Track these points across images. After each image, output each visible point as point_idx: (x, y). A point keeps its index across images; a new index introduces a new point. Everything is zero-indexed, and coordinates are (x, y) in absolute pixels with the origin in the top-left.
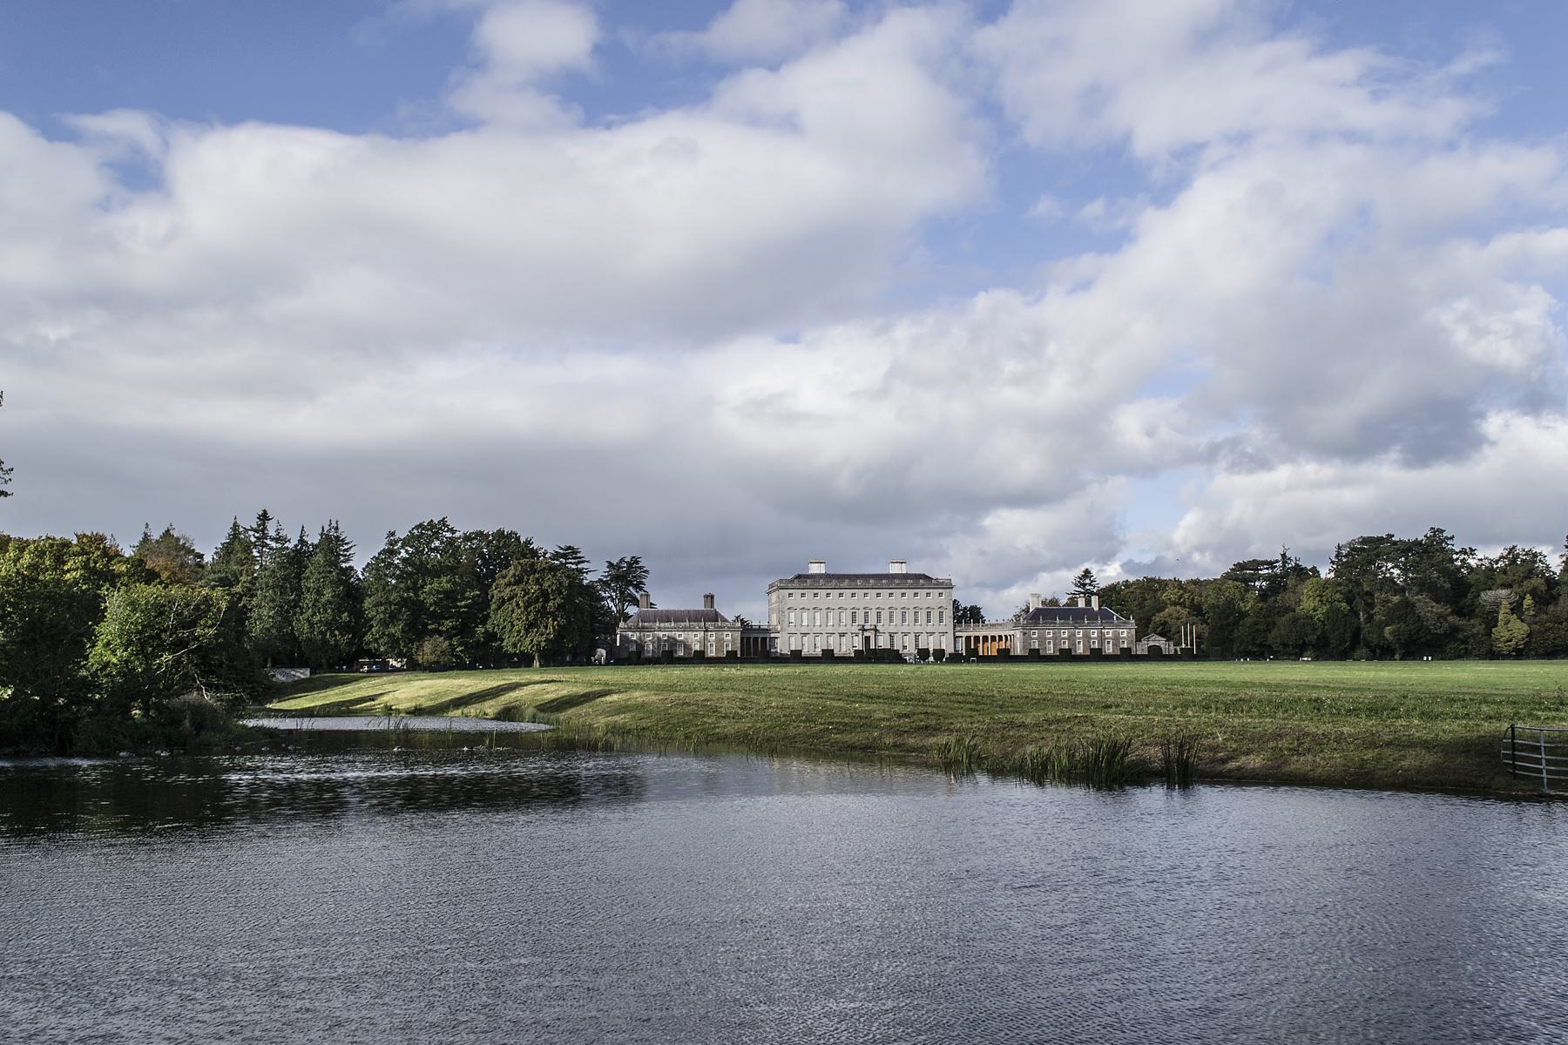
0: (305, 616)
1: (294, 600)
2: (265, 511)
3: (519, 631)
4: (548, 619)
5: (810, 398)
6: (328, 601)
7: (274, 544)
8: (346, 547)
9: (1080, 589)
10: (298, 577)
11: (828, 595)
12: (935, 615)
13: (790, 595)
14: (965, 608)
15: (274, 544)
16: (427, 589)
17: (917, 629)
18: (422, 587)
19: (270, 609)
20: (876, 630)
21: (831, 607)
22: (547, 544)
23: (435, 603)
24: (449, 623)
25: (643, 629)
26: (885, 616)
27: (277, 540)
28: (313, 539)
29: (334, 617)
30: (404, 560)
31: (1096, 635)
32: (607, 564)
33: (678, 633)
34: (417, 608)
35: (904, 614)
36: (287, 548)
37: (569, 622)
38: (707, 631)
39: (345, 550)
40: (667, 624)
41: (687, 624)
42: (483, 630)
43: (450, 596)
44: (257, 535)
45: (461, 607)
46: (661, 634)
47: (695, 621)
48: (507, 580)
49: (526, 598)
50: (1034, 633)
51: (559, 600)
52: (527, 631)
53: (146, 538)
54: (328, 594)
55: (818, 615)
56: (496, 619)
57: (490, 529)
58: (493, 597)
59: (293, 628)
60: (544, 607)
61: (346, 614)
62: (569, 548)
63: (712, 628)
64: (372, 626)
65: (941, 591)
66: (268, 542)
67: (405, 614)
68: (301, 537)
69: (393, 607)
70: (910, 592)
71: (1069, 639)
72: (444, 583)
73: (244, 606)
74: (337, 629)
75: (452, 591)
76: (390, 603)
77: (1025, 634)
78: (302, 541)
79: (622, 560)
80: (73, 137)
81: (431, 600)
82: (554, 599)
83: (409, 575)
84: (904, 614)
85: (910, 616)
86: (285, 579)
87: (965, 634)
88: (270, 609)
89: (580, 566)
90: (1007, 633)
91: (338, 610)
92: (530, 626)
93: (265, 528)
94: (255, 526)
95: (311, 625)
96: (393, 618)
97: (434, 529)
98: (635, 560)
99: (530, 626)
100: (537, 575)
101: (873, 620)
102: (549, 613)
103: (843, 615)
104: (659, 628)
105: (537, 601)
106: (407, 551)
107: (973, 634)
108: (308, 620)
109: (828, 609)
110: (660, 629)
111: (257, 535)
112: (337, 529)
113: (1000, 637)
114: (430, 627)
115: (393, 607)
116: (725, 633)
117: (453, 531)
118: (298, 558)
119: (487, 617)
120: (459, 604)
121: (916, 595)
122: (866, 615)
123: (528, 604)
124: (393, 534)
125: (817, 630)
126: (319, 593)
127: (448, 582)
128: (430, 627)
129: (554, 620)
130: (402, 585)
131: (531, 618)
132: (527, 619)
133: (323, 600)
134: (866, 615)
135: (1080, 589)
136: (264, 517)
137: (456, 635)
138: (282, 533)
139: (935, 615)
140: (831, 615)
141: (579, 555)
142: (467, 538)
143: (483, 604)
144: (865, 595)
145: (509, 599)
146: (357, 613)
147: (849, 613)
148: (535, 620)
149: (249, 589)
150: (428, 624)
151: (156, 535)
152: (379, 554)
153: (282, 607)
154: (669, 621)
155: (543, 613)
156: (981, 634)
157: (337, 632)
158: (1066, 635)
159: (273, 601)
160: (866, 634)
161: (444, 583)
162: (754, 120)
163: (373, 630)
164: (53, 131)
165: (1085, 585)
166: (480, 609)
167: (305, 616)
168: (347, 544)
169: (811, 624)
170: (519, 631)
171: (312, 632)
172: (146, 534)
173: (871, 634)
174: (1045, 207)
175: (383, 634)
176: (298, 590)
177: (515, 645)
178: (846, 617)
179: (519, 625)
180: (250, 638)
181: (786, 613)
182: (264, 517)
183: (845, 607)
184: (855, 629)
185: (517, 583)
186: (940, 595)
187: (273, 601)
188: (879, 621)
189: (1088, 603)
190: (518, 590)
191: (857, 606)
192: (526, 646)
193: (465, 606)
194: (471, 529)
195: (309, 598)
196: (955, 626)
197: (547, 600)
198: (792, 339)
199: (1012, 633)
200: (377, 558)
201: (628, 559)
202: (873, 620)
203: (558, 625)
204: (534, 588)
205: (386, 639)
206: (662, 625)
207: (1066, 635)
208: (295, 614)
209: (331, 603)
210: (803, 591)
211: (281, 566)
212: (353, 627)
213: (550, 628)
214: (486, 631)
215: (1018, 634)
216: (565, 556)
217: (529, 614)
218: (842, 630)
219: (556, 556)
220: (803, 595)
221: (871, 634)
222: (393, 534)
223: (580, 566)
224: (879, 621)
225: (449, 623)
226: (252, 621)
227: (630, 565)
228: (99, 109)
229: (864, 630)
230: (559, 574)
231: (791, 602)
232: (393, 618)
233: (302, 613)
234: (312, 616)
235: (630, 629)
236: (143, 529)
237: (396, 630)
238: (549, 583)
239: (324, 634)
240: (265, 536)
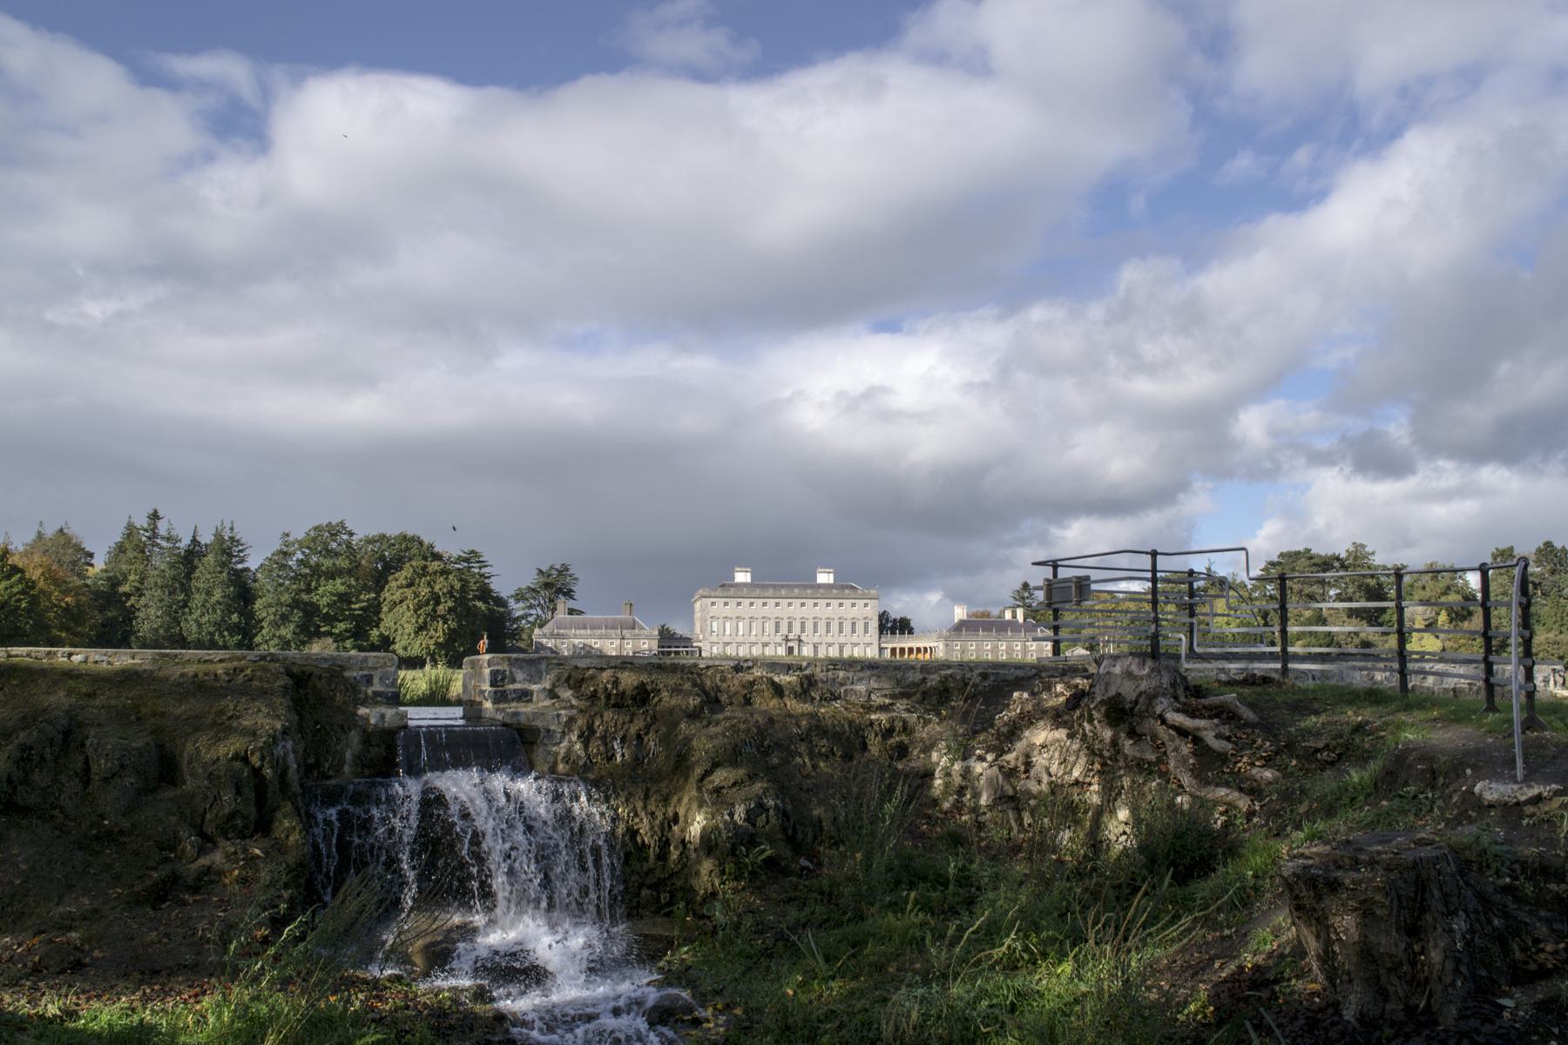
0: (194, 617)
1: (183, 600)
2: (156, 511)
3: (409, 635)
4: (438, 622)
5: (907, 396)
6: (217, 601)
7: (164, 544)
8: (240, 548)
9: (1018, 603)
10: (188, 577)
11: (752, 604)
12: (860, 626)
13: (713, 604)
14: (895, 620)
15: (164, 544)
16: (321, 589)
17: (842, 640)
18: (316, 589)
19: (158, 609)
20: (800, 641)
21: (756, 616)
22: (450, 547)
23: (328, 605)
24: (342, 626)
25: (558, 636)
26: (809, 626)
27: (168, 539)
28: (206, 538)
29: (223, 618)
30: (300, 562)
31: (1019, 648)
32: (537, 571)
33: (593, 641)
34: (310, 610)
35: (828, 625)
36: (179, 548)
37: (461, 626)
38: (623, 638)
39: (240, 551)
40: (583, 632)
41: (589, 632)
42: (378, 633)
43: (344, 598)
44: (146, 534)
45: (355, 610)
46: (576, 641)
47: (611, 628)
48: (399, 583)
49: (416, 601)
50: (957, 645)
51: (450, 604)
52: (416, 633)
53: (40, 535)
54: (218, 595)
55: (741, 624)
56: (388, 622)
57: (392, 531)
58: (385, 599)
59: (181, 628)
60: (435, 611)
61: (236, 615)
62: (472, 552)
63: (628, 636)
64: (262, 628)
65: (866, 601)
66: (159, 541)
67: (297, 615)
68: (194, 537)
69: (284, 609)
70: (835, 603)
71: (992, 651)
72: (339, 585)
73: (133, 606)
74: (227, 629)
75: (346, 594)
76: (282, 604)
77: (947, 645)
78: (194, 541)
79: (552, 567)
80: (172, 84)
81: (324, 601)
82: (446, 602)
83: (305, 576)
84: (828, 625)
85: (835, 627)
86: (174, 579)
87: (890, 646)
88: (158, 609)
89: (483, 570)
90: (932, 645)
91: (229, 611)
92: (422, 628)
93: (156, 528)
94: (145, 526)
95: (200, 625)
96: (285, 618)
97: (335, 530)
98: (885, 612)
99: (422, 628)
100: (428, 578)
101: (797, 630)
102: (439, 616)
103: (767, 625)
104: (575, 635)
105: (427, 604)
106: (303, 553)
107: (898, 646)
108: (196, 621)
109: (752, 618)
110: (576, 637)
111: (146, 534)
112: (232, 529)
113: (925, 649)
114: (322, 629)
115: (284, 609)
116: (642, 641)
117: (351, 534)
118: (191, 557)
119: (380, 620)
120: (353, 606)
121: (841, 605)
122: (790, 625)
123: (419, 607)
124: (287, 535)
125: (740, 639)
126: (209, 593)
127: (342, 584)
128: (322, 629)
129: (445, 623)
130: (295, 587)
131: (421, 620)
132: (417, 622)
133: (213, 600)
134: (790, 625)
135: (1018, 603)
136: (155, 516)
137: (348, 638)
138: (174, 533)
139: (860, 626)
140: (754, 625)
141: (481, 559)
142: (370, 541)
143: (374, 609)
144: (790, 604)
145: (401, 602)
146: (248, 615)
147: (773, 622)
148: (425, 623)
149: (138, 589)
150: (320, 627)
151: (50, 531)
152: (273, 555)
153: (171, 607)
154: (585, 628)
155: (434, 616)
156: (906, 645)
157: (226, 633)
158: (1034, 648)
159: (161, 601)
160: (790, 644)
161: (339, 585)
162: (938, 58)
163: (264, 631)
164: (148, 78)
165: (1023, 598)
166: (372, 614)
167: (194, 617)
168: (242, 545)
169: (734, 634)
170: (409, 635)
171: (200, 633)
172: (39, 532)
173: (794, 644)
174: (1243, 164)
175: (274, 635)
176: (186, 590)
177: (405, 649)
178: (770, 626)
179: (409, 628)
180: (138, 638)
181: (709, 622)
182: (155, 516)
183: (769, 616)
184: (779, 639)
185: (409, 585)
186: (866, 605)
187: (161, 601)
188: (803, 631)
189: (1014, 616)
190: (409, 592)
191: (781, 616)
192: (415, 650)
193: (360, 609)
194: (373, 532)
195: (198, 599)
196: (880, 638)
197: (438, 603)
198: (890, 327)
199: (935, 644)
200: (270, 559)
201: (558, 567)
202: (797, 630)
203: (449, 628)
204: (424, 591)
205: (276, 641)
206: (578, 632)
207: (989, 647)
208: (184, 614)
209: (220, 604)
210: (725, 600)
211: (172, 566)
212: (244, 628)
213: (439, 631)
214: (381, 635)
215: (941, 646)
216: (467, 560)
217: (419, 617)
218: (765, 639)
219: (460, 559)
220: (726, 604)
221: (794, 644)
222: (287, 535)
223: (483, 570)
224: (803, 631)
225: (342, 626)
226: (140, 620)
227: (560, 572)
228: (194, 48)
229: (787, 640)
230: (451, 577)
231: (714, 610)
232: (285, 618)
233: (191, 613)
234: (201, 616)
235: (545, 636)
236: (37, 527)
237: (287, 631)
238: (441, 586)
239: (212, 634)
240: (155, 535)
